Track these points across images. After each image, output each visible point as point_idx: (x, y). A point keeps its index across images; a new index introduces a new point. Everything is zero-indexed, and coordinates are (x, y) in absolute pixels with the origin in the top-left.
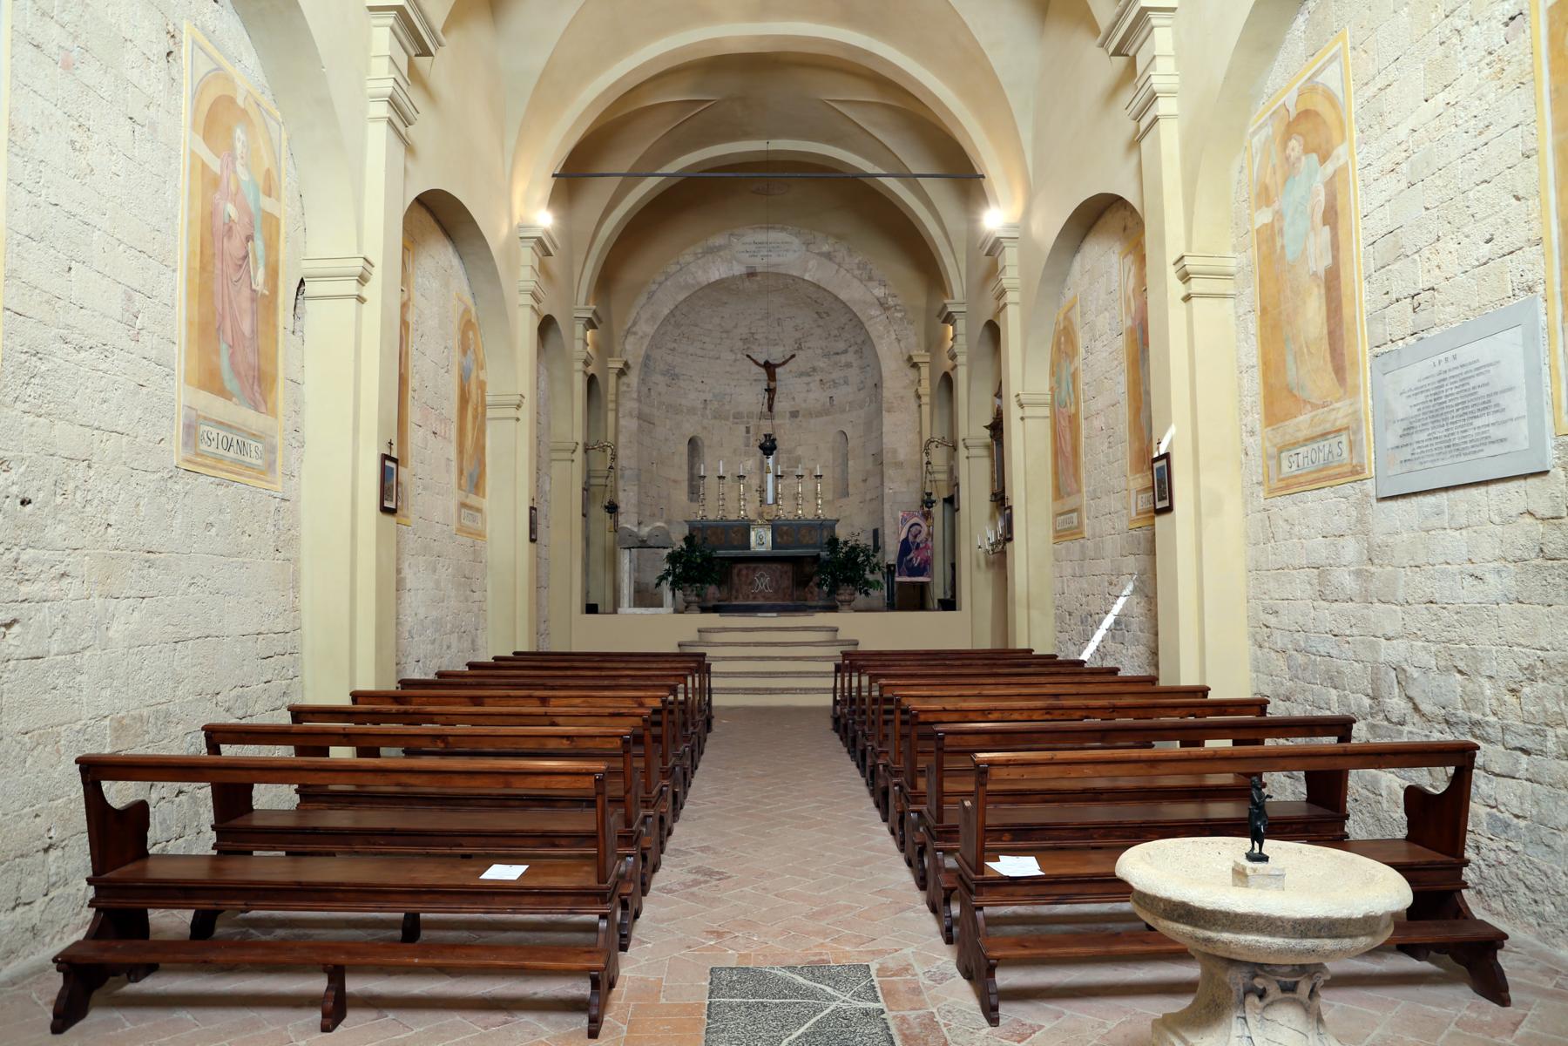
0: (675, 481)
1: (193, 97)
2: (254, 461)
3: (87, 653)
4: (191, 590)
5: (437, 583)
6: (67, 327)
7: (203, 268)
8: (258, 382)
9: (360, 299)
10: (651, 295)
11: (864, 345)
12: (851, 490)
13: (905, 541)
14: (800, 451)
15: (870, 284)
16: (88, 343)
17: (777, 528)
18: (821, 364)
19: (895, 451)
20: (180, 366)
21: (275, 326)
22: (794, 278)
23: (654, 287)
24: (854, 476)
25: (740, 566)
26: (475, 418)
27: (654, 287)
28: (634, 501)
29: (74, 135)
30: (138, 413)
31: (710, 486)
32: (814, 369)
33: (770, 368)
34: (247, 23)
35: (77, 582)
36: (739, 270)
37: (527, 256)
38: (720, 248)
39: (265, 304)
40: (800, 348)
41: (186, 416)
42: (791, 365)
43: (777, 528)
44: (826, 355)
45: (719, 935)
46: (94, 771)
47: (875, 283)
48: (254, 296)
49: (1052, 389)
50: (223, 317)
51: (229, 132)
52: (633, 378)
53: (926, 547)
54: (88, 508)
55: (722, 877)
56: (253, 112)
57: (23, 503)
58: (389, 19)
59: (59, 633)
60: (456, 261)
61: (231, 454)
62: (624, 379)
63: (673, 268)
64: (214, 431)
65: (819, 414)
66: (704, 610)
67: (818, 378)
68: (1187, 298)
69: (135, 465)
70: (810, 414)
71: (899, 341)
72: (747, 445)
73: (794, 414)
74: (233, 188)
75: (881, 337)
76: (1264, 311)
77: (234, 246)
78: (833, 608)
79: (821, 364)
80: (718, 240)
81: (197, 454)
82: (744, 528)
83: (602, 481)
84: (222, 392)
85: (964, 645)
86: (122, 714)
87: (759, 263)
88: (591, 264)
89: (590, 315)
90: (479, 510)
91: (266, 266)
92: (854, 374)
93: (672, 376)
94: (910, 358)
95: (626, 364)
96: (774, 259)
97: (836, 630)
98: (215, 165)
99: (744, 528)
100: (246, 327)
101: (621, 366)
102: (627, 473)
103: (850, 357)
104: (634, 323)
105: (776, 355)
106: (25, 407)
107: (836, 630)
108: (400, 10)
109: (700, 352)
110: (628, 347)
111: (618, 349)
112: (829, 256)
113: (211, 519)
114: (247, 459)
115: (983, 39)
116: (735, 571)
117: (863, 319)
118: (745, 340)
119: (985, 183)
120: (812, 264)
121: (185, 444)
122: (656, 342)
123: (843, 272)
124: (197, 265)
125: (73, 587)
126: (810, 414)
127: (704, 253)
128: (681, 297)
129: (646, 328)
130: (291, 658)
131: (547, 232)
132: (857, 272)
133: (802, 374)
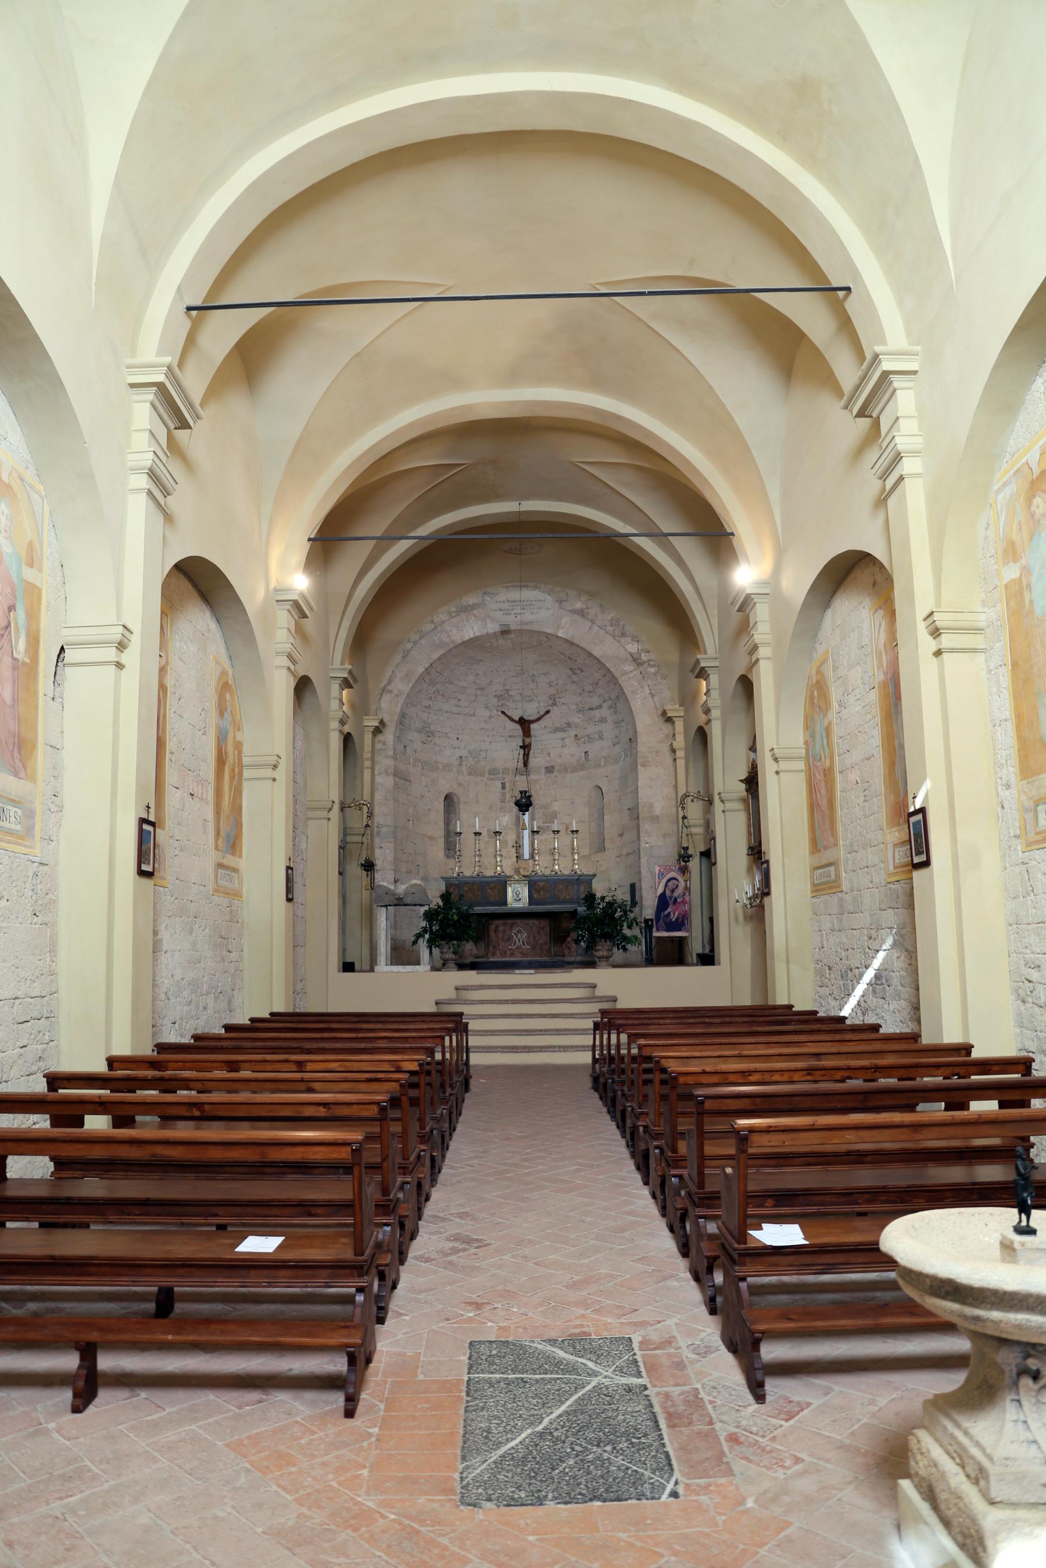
0: (431, 838)
2: (13, 826)
5: (194, 944)
9: (119, 666)
10: (406, 654)
11: (619, 700)
12: (607, 845)
13: (663, 895)
14: (556, 806)
15: (623, 640)
18: (577, 719)
19: (651, 805)
24: (611, 831)
25: (497, 922)
26: (232, 778)
27: (409, 646)
32: (569, 725)
33: (524, 724)
36: (492, 628)
37: (284, 619)
38: (474, 607)
40: (554, 704)
43: (533, 884)
45: (478, 1306)
47: (629, 639)
49: (806, 743)
52: (389, 736)
53: (684, 902)
55: (481, 1244)
58: (150, 395)
60: (213, 625)
62: (380, 737)
65: (574, 770)
67: (572, 733)
68: (938, 653)
70: (566, 769)
71: (653, 696)
72: (503, 801)
73: (550, 770)
75: (635, 693)
76: (1015, 665)
78: (591, 964)
79: (577, 719)
80: (471, 599)
82: (501, 884)
83: (358, 839)
87: (512, 621)
88: (346, 624)
89: (346, 675)
90: (235, 870)
92: (608, 729)
94: (664, 713)
95: (382, 722)
96: (528, 617)
97: (595, 987)
99: (501, 884)
102: (384, 830)
104: (390, 682)
105: (530, 711)
107: (595, 987)
108: (160, 387)
109: (455, 709)
110: (383, 705)
111: (373, 707)
112: (581, 613)
115: (729, 401)
116: (493, 927)
117: (617, 675)
118: (499, 697)
119: (735, 541)
120: (565, 620)
122: (411, 699)
123: (596, 629)
126: (566, 769)
127: (458, 612)
128: (436, 655)
129: (402, 686)
131: (302, 595)
132: (610, 629)
133: (556, 730)
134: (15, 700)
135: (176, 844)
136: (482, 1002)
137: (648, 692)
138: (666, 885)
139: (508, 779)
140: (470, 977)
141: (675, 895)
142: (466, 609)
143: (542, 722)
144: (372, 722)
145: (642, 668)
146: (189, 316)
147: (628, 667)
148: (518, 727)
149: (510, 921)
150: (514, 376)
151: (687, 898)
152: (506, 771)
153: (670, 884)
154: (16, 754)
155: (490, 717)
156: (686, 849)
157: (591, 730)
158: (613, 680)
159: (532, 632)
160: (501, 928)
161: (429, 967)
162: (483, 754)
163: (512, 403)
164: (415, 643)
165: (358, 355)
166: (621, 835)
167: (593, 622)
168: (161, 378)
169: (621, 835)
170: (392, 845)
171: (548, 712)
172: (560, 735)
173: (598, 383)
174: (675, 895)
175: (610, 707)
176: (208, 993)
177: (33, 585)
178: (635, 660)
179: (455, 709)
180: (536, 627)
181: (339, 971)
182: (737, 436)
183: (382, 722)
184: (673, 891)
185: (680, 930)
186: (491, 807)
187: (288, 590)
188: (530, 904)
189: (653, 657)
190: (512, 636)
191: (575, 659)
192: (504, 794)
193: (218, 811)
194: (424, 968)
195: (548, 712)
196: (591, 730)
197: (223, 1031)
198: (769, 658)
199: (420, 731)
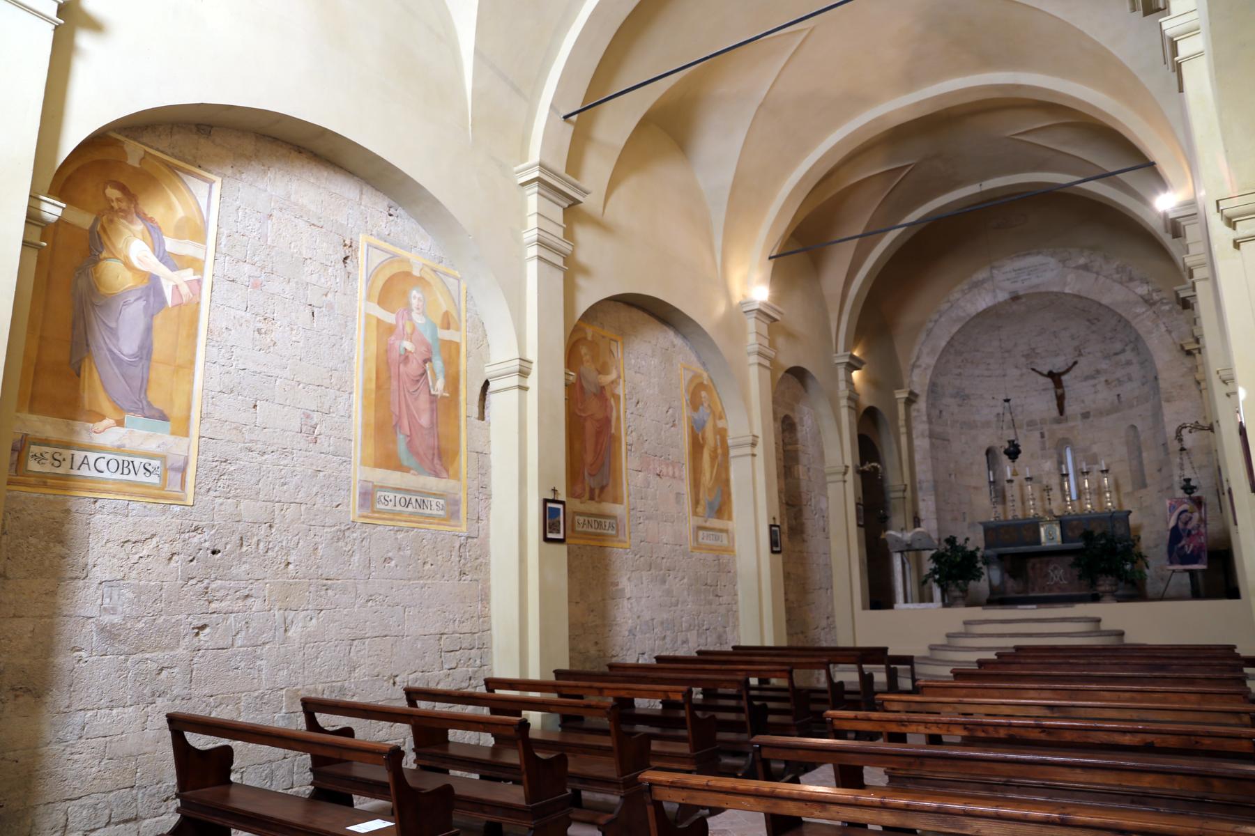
0: (975, 488)
1: (367, 280)
2: (435, 512)
3: (267, 646)
4: (370, 604)
5: (669, 593)
6: (251, 441)
7: (378, 387)
8: (440, 457)
9: (523, 388)
10: (929, 332)
11: (1137, 343)
12: (1148, 481)
13: (1175, 528)
14: (1095, 449)
15: (1131, 285)
16: (270, 449)
17: (1064, 522)
18: (1104, 365)
20: (356, 453)
21: (457, 417)
22: (1056, 294)
23: (931, 325)
24: (1150, 468)
25: (1033, 560)
26: (713, 458)
27: (931, 325)
28: (932, 507)
29: (259, 325)
30: (315, 490)
31: (1012, 491)
32: (1098, 372)
33: (1056, 377)
34: (419, 221)
35: (259, 602)
36: (1002, 296)
37: (751, 323)
38: (983, 281)
39: (445, 406)
40: (1080, 355)
41: (362, 487)
42: (1076, 371)
43: (1064, 522)
44: (1107, 357)
46: (178, 725)
47: (1137, 283)
48: (433, 399)
50: (400, 417)
51: (405, 294)
52: (922, 404)
53: (1199, 534)
54: (270, 553)
56: (429, 276)
57: (214, 552)
58: (535, 188)
59: (243, 633)
60: (678, 341)
61: (410, 509)
62: (914, 406)
63: (945, 306)
64: (391, 496)
65: (1109, 412)
66: (969, 605)
67: (1103, 379)
68: (1237, 245)
69: (313, 523)
70: (1101, 413)
71: (1169, 332)
72: (1043, 448)
73: (1086, 416)
74: (408, 329)
75: (1150, 332)
77: (413, 368)
78: (1095, 598)
79: (1104, 365)
80: (981, 275)
81: (374, 512)
82: (1034, 525)
83: (900, 494)
84: (399, 467)
85: (756, 643)
86: (299, 687)
87: (1020, 287)
88: (845, 318)
89: (847, 360)
90: (726, 531)
91: (446, 377)
92: (1135, 370)
93: (963, 397)
94: (1182, 347)
95: (911, 393)
96: (1035, 280)
97: (1098, 621)
98: (390, 318)
99: (1034, 525)
100: (424, 420)
101: (906, 395)
102: (925, 485)
103: (1129, 355)
104: (918, 358)
105: (1058, 364)
106: (217, 494)
107: (1098, 621)
108: (538, 179)
109: (986, 373)
110: (915, 379)
111: (906, 381)
112: (1086, 268)
113: (390, 554)
114: (428, 511)
115: (1102, 38)
116: (1030, 565)
117: (1129, 318)
118: (1027, 356)
120: (1071, 277)
121: (362, 506)
122: (938, 370)
123: (1102, 279)
124: (373, 385)
125: (256, 604)
126: (1101, 413)
127: (970, 289)
128: (955, 329)
129: (928, 361)
130: (479, 652)
131: (765, 304)
132: (1116, 276)
133: (1087, 378)
134: (434, 424)
135: (639, 514)
136: (982, 636)
137: (1163, 329)
138: (1178, 518)
139: (1046, 429)
140: (977, 613)
141: (1189, 526)
142: (977, 285)
143: (1072, 373)
144: (901, 395)
145: (1155, 308)
146: (570, 122)
147: (1140, 309)
148: (1049, 380)
149: (1046, 559)
150: (910, 80)
151: (1203, 530)
152: (1043, 421)
153: (1183, 516)
154: (436, 461)
155: (1022, 375)
156: (1188, 480)
157: (1120, 373)
158: (1127, 324)
159: (1040, 293)
160: (1038, 566)
161: (940, 604)
162: (1020, 409)
163: (918, 104)
164: (936, 321)
165: (761, 105)
166: (1160, 470)
167: (1098, 273)
168: (536, 174)
169: (1160, 470)
170: (933, 498)
171: (1075, 363)
172: (1092, 382)
173: (987, 62)
174: (1189, 526)
175: (1133, 350)
176: (688, 630)
177: (450, 342)
178: (1146, 301)
179: (986, 373)
180: (1043, 289)
181: (864, 608)
182: (1121, 67)
183: (911, 393)
184: (1186, 523)
185: (1196, 563)
186: (1032, 456)
187: (753, 302)
188: (1063, 541)
189: (1165, 295)
190: (1024, 300)
191: (1088, 312)
192: (1043, 443)
193: (696, 484)
194: (937, 603)
195: (1075, 363)
196: (1120, 373)
197: (654, 661)
198: (1206, 279)
199: (954, 396)
